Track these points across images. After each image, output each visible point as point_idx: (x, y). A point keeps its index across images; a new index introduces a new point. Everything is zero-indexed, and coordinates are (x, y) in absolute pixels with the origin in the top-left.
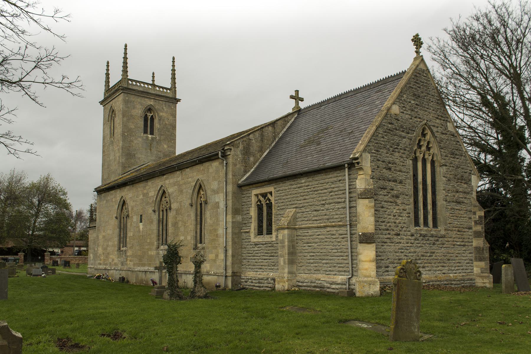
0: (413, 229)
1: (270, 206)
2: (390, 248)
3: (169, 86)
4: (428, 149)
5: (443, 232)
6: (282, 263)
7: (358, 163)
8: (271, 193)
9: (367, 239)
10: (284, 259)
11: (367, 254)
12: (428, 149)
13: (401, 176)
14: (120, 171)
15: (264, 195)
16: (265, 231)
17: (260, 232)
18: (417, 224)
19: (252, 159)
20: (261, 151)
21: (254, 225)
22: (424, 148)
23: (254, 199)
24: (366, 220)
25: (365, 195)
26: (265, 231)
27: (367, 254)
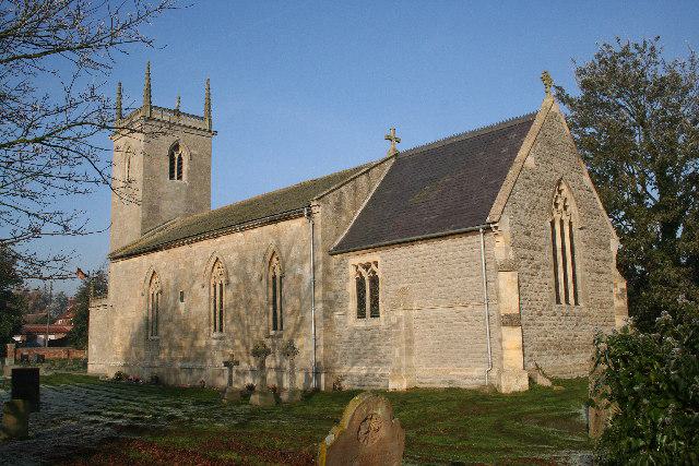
0: (555, 308)
1: (374, 280)
2: (532, 331)
3: (202, 114)
4: (565, 208)
5: (585, 310)
6: (397, 354)
7: (496, 228)
8: (376, 263)
9: (511, 321)
10: (401, 350)
11: (512, 337)
12: (565, 208)
13: (540, 242)
14: (138, 230)
15: (367, 267)
16: (368, 312)
17: (361, 314)
18: (558, 302)
19: (344, 219)
20: (355, 208)
21: (352, 305)
22: (560, 207)
23: (352, 271)
24: (510, 301)
25: (507, 267)
26: (368, 312)
27: (512, 337)
